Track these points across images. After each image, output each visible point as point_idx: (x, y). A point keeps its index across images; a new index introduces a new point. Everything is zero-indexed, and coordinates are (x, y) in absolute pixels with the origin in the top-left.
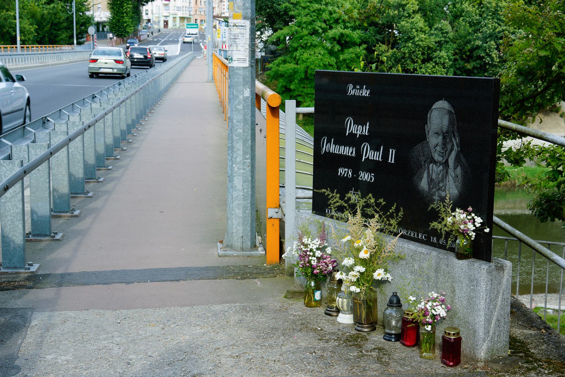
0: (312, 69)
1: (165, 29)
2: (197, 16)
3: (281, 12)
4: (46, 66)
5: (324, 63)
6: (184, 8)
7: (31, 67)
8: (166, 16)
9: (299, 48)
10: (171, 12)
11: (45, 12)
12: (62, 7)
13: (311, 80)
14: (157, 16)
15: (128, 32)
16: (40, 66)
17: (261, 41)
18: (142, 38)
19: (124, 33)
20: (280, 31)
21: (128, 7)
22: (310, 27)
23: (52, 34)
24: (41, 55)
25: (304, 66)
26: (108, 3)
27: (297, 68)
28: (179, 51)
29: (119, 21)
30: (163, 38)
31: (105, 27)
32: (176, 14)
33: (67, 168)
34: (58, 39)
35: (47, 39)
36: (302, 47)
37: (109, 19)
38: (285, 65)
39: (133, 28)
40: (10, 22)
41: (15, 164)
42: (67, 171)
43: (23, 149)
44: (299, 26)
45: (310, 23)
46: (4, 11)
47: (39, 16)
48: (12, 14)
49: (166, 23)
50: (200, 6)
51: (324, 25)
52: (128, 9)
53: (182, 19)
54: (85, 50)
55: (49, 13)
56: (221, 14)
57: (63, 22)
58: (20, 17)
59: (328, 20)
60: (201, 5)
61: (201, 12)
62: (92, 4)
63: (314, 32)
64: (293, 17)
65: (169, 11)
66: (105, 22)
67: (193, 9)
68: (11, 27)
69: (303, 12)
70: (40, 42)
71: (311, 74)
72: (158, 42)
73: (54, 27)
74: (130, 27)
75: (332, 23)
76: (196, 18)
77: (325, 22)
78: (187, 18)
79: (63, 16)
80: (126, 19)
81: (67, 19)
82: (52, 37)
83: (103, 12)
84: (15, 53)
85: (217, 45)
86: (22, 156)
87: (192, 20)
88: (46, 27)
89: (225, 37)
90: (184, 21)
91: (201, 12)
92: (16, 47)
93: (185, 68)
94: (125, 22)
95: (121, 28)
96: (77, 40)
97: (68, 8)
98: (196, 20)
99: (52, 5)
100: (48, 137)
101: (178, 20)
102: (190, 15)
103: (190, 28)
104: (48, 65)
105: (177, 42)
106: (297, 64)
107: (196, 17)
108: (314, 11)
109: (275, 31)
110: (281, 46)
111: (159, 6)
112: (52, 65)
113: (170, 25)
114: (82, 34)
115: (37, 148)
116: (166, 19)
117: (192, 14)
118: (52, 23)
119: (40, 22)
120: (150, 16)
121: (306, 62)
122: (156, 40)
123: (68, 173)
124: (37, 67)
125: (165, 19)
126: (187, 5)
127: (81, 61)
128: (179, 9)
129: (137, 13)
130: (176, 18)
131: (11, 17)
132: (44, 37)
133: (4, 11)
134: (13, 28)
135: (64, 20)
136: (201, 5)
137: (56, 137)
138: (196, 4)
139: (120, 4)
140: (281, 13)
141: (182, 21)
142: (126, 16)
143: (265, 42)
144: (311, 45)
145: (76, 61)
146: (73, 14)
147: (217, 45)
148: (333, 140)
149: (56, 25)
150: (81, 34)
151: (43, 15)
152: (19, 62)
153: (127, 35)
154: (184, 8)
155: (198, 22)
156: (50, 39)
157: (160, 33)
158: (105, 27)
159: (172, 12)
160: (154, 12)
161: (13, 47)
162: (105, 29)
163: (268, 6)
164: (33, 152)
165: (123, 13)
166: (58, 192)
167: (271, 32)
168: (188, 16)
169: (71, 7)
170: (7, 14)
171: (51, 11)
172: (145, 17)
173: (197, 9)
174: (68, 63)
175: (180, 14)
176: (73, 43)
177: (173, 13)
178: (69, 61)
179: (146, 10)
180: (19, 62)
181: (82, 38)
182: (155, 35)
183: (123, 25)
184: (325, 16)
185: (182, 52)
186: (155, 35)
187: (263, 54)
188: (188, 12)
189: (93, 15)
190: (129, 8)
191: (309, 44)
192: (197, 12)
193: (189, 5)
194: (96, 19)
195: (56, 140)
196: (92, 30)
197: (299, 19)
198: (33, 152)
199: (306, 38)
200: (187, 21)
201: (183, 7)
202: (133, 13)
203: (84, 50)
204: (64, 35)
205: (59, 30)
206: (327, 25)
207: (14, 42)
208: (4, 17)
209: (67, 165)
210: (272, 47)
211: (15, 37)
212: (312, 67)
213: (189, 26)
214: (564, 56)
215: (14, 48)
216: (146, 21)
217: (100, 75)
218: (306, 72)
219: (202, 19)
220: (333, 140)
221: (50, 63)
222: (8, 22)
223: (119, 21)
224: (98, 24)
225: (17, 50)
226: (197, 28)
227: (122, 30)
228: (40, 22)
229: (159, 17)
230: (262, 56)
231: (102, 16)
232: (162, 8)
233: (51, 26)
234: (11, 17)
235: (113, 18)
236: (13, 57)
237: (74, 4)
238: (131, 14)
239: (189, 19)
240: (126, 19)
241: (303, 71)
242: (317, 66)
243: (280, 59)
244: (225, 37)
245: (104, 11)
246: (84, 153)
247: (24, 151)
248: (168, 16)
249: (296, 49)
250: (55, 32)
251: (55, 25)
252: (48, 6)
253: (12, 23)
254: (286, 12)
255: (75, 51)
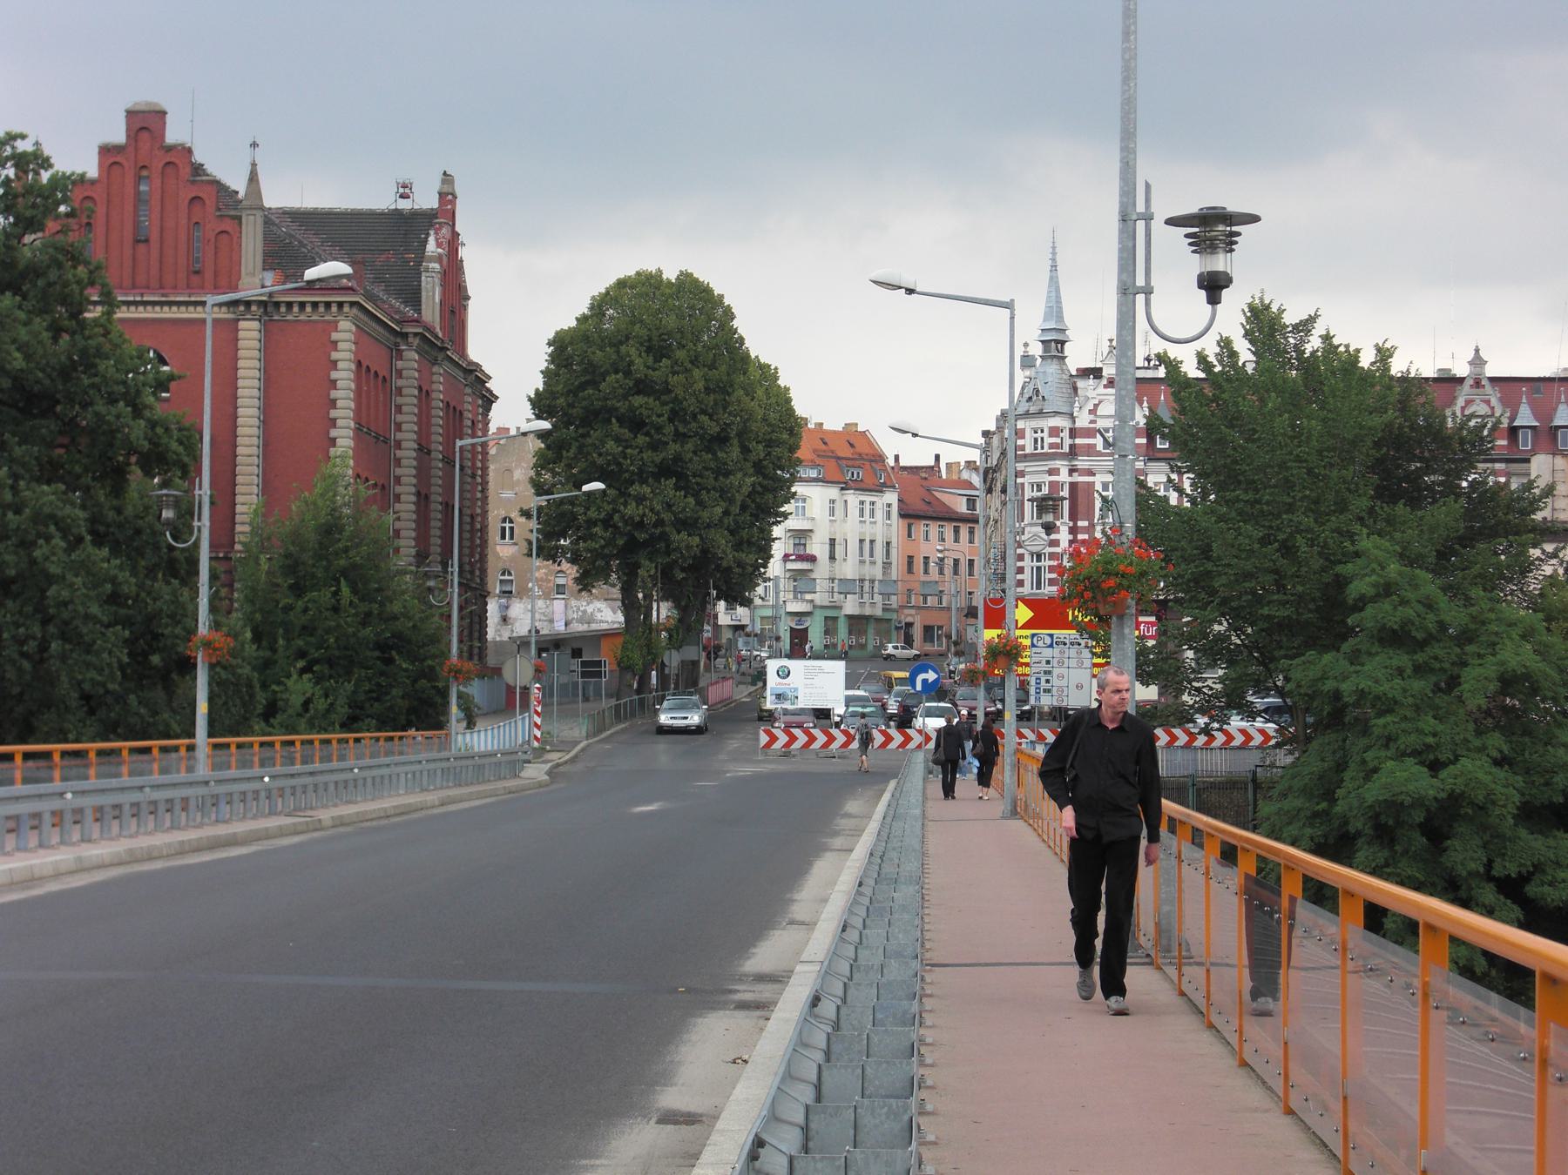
50: (923, 578)
78: (878, 620)
89: (1049, 691)
116: (799, 622)
117: (895, 606)
126: (878, 572)
148: (654, 673)
159: (820, 598)
166: (89, 263)
175: (851, 606)
214: (1566, 620)
217: (197, 479)
219: (927, 623)
220: (654, 673)
229: (774, 619)
244: (1049, 691)
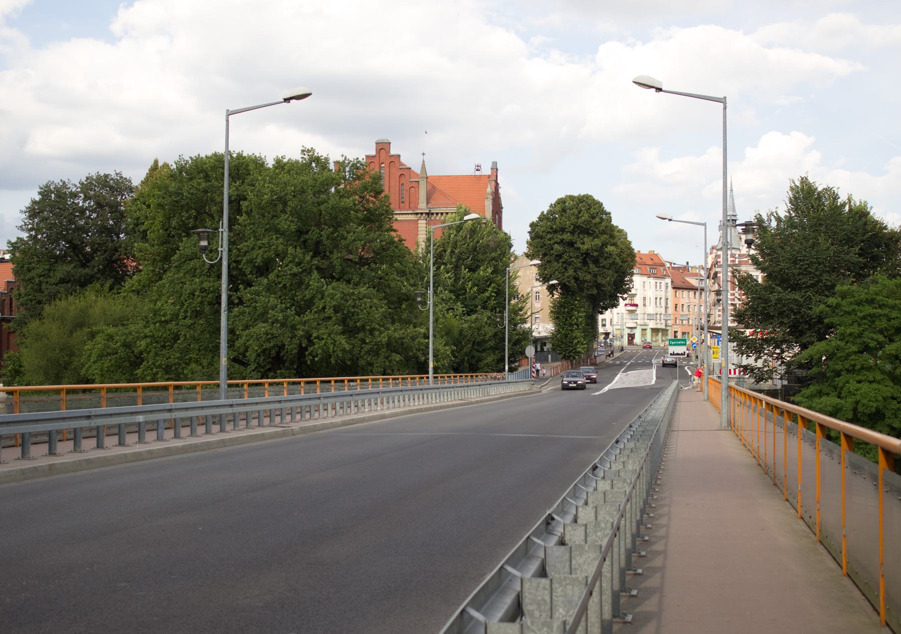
0: (864, 405)
1: (631, 347)
2: (678, 327)
3: (812, 318)
4: (468, 404)
5: (884, 395)
6: (658, 316)
7: (448, 407)
8: (631, 328)
9: (843, 373)
10: (639, 322)
11: (464, 325)
12: (489, 318)
13: (864, 422)
14: (619, 327)
15: (580, 352)
16: (461, 405)
17: (783, 362)
18: (598, 360)
19: (572, 354)
20: (811, 348)
21: (580, 316)
22: (858, 341)
23: (473, 357)
24: (461, 389)
25: (850, 400)
26: (552, 312)
27: (841, 403)
28: (654, 378)
29: (566, 336)
30: (629, 360)
31: (545, 345)
32: (646, 325)
33: (599, 611)
34: (481, 364)
35: (466, 364)
36: (848, 371)
37: (553, 333)
38: (822, 399)
39: (586, 346)
40: (419, 342)
41: (552, 628)
42: (599, 617)
43: (541, 586)
44: (841, 340)
45: (860, 335)
46: (411, 327)
47: (456, 332)
48: (423, 331)
49: (631, 337)
50: (682, 313)
51: (881, 338)
52: (580, 320)
53: (655, 331)
54: (521, 380)
55: (470, 327)
56: (715, 323)
57: (489, 340)
58: (434, 336)
59: (886, 329)
60: (683, 311)
61: (682, 320)
62: (529, 313)
63: (866, 349)
64: (831, 326)
65: (636, 321)
66: (546, 338)
67: (672, 317)
68: (419, 350)
69: (847, 319)
70: (457, 369)
71: (863, 412)
72: (622, 365)
73: (476, 347)
74: (583, 344)
75: (892, 335)
76: (676, 330)
77: (881, 332)
78: (663, 330)
79: (490, 331)
80: (577, 333)
81: (496, 334)
82: (473, 362)
83: (541, 325)
84: (426, 386)
85: (712, 369)
86: (539, 598)
87: (669, 332)
88: (465, 348)
90: (657, 335)
91: (682, 320)
92: (428, 378)
93: (675, 405)
94: (576, 338)
95: (569, 346)
96: (509, 365)
97: (498, 320)
98: (676, 332)
99: (474, 317)
100: (568, 555)
101: (649, 332)
102: (666, 326)
103: (674, 345)
104: (472, 403)
105: (650, 365)
106: (839, 397)
107: (676, 328)
108: (864, 318)
109: (804, 347)
110: (815, 370)
111: (623, 314)
112: (477, 402)
113: (638, 340)
114: (517, 355)
115: (567, 584)
117: (670, 324)
118: (474, 342)
119: (456, 339)
120: (608, 328)
121: (855, 395)
122: (618, 362)
123: (599, 620)
124: (457, 405)
125: (629, 331)
126: (663, 310)
127: (516, 395)
128: (651, 317)
129: (592, 323)
130: (646, 330)
131: (420, 336)
132: (462, 361)
133: (411, 327)
134: (423, 350)
135: (490, 337)
136: (683, 311)
137: (581, 555)
138: (676, 310)
139: (568, 312)
140: (813, 320)
141: (654, 334)
142: (576, 329)
143: (789, 365)
144: (862, 368)
145: (509, 397)
146: (505, 328)
147: (712, 369)
149: (479, 344)
150: (514, 357)
151: (461, 331)
152: (432, 398)
153: (577, 357)
154: (658, 316)
155: (679, 336)
156: (471, 365)
157: (623, 352)
158: (545, 345)
160: (615, 322)
161: (423, 378)
162: (545, 349)
163: (793, 311)
164: (559, 590)
165: (571, 325)
167: (797, 349)
168: (663, 327)
169: (502, 318)
170: (416, 332)
171: (473, 325)
172: (601, 330)
173: (676, 316)
174: (498, 399)
175: (652, 325)
176: (504, 370)
177: (642, 323)
178: (499, 396)
179: (603, 320)
180: (432, 398)
181: (515, 362)
182: (616, 355)
183: (572, 342)
184: (882, 324)
185: (659, 381)
186: (616, 355)
187: (785, 383)
188: (663, 321)
189: (531, 328)
190: (581, 317)
191: (858, 367)
192: (678, 321)
193: (666, 311)
194: (535, 334)
195: (581, 560)
196: (530, 351)
197: (841, 329)
198: (559, 590)
199: (853, 357)
200: (663, 335)
201: (656, 314)
202: (587, 325)
203: (519, 380)
204: (490, 359)
205: (484, 350)
206: (885, 337)
207: (422, 369)
208: (411, 335)
209: (599, 606)
210: (800, 373)
211: (426, 362)
212: (865, 401)
213: (673, 343)
215: (425, 378)
216: (603, 336)
218: (855, 410)
221: (473, 400)
222: (416, 343)
223: (566, 336)
224: (536, 341)
225: (429, 381)
226: (685, 345)
227: (571, 349)
228: (456, 339)
229: (621, 330)
230: (783, 386)
231: (540, 329)
232: (626, 316)
233: (473, 345)
234: (420, 336)
235: (558, 331)
236: (424, 391)
237: (506, 314)
238: (583, 325)
239: (664, 331)
240: (577, 333)
241: (851, 408)
242: (874, 400)
243: (813, 388)
245: (544, 322)
246: (612, 576)
247: (544, 588)
248: (635, 328)
249: (838, 374)
250: (478, 354)
251: (479, 345)
252: (469, 318)
253: (422, 343)
254: (820, 320)
255: (507, 381)
